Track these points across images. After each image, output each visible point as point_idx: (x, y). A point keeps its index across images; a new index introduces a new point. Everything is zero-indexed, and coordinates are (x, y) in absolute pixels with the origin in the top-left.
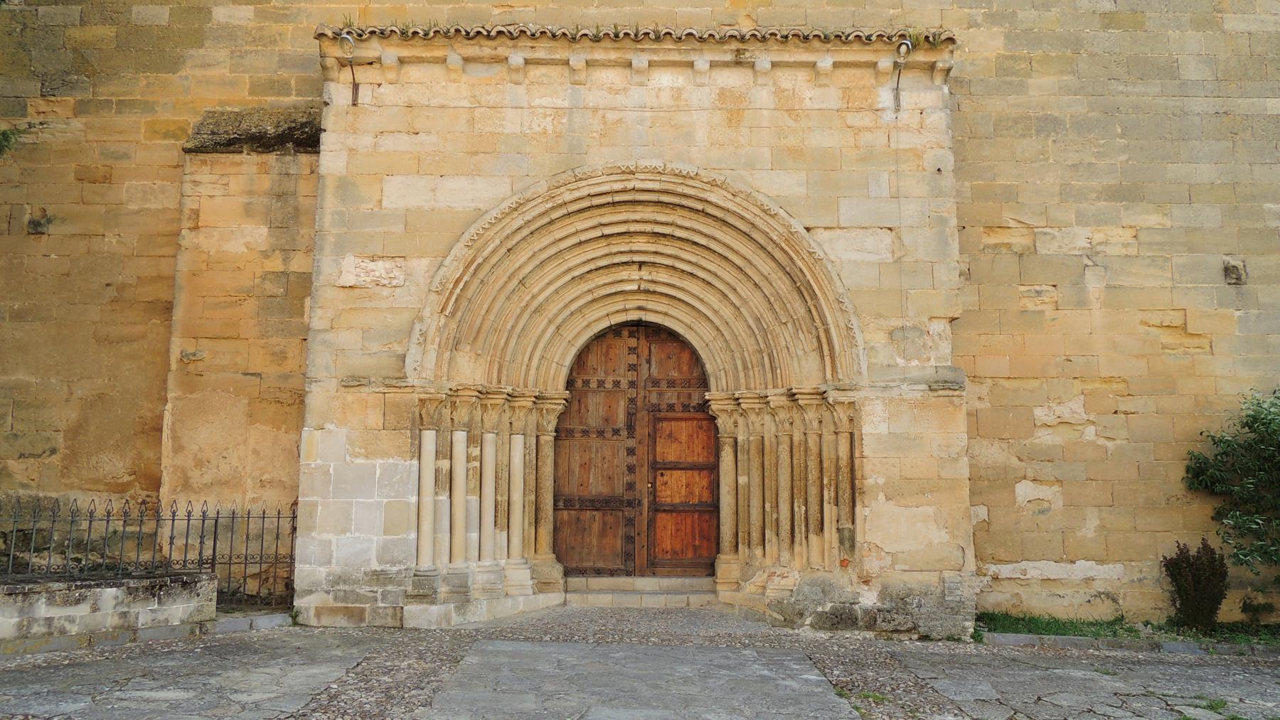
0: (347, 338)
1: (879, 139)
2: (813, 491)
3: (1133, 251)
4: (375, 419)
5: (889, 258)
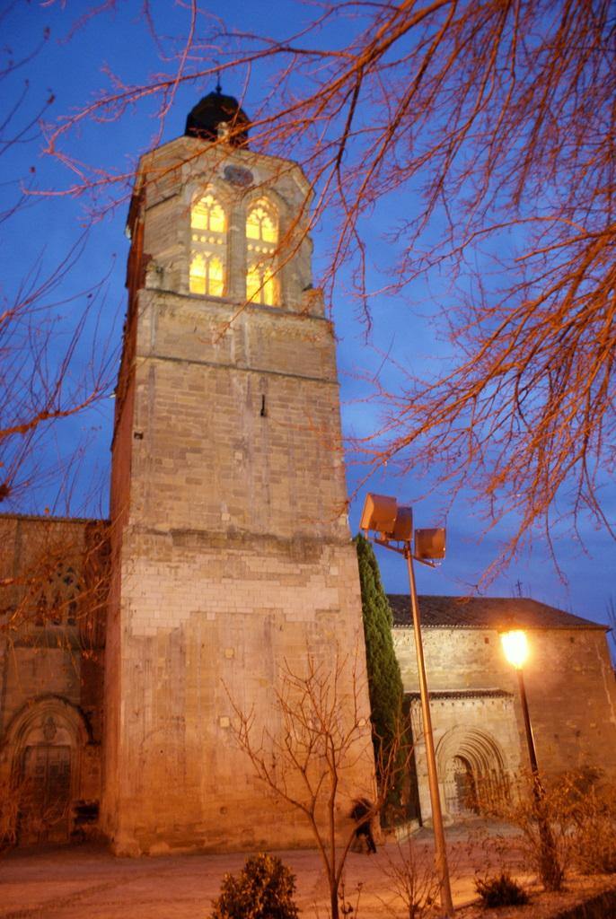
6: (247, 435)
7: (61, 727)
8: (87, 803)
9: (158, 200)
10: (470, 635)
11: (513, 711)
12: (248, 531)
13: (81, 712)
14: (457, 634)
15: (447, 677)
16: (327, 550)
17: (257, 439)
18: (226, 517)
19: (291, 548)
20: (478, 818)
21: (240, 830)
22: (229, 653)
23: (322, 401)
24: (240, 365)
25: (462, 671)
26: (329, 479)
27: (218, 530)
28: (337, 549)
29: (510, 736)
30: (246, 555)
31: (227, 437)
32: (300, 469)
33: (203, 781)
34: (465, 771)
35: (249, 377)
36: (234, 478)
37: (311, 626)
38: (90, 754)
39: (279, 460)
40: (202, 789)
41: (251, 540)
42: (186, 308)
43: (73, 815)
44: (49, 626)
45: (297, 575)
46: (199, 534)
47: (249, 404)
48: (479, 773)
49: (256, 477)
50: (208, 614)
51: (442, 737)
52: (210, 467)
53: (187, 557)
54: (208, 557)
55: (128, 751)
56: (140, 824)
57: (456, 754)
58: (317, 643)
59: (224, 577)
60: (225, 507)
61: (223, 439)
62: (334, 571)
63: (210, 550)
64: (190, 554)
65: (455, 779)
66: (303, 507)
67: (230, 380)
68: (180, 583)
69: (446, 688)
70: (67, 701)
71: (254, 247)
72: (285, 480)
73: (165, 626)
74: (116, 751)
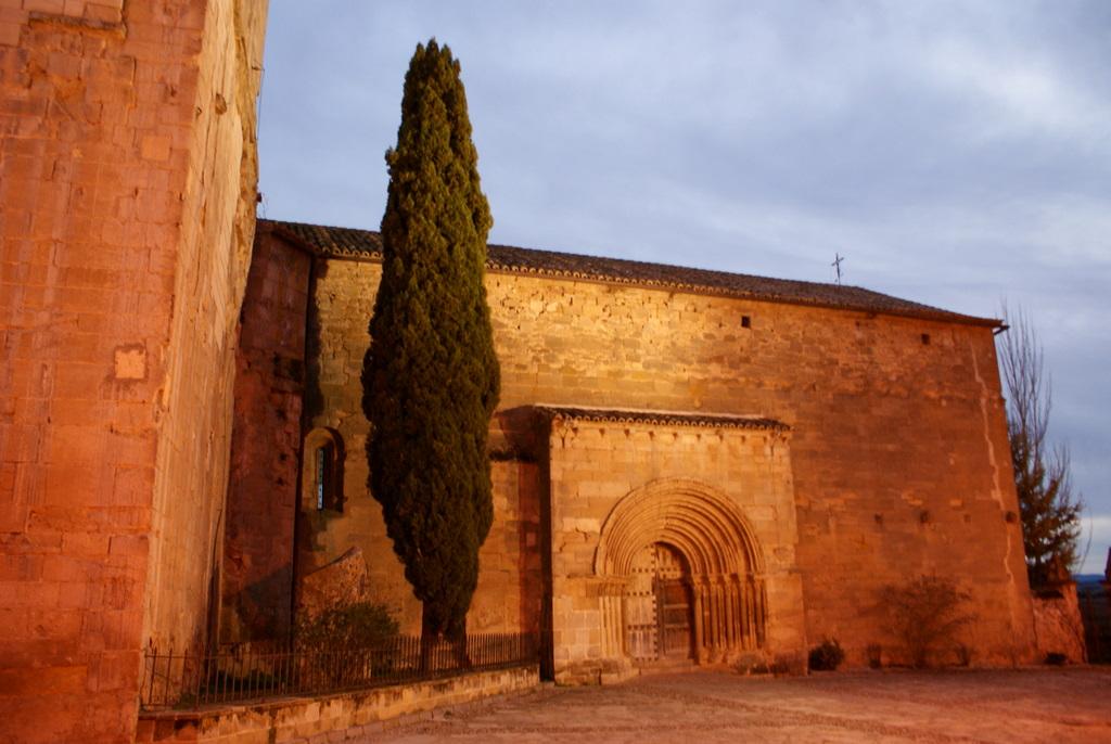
0: (568, 556)
1: (767, 469)
2: (744, 617)
3: (844, 509)
4: (582, 593)
5: (771, 518)
11: (786, 460)
25: (686, 376)
29: (774, 507)
34: (678, 574)
48: (705, 579)
51: (622, 499)
57: (659, 539)
69: (648, 406)
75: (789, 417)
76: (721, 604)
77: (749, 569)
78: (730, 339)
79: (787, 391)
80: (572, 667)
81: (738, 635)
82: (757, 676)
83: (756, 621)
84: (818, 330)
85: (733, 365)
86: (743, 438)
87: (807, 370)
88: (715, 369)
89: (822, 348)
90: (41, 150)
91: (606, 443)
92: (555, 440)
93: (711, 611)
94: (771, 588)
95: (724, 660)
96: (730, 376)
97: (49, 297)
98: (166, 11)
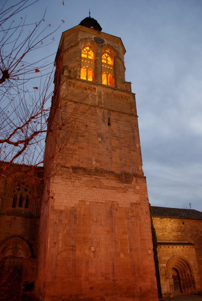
0: (162, 271)
6: (103, 132)
7: (20, 249)
8: (29, 282)
9: (69, 47)
10: (177, 221)
11: (195, 251)
12: (103, 169)
13: (28, 243)
14: (172, 220)
15: (169, 236)
16: (134, 179)
17: (106, 134)
18: (94, 163)
19: (120, 177)
20: (182, 294)
21: (99, 298)
22: (95, 219)
23: (131, 122)
24: (100, 105)
25: (175, 234)
26: (135, 151)
27: (91, 168)
28: (138, 179)
29: (194, 261)
30: (103, 179)
31: (95, 132)
32: (123, 147)
33: (83, 275)
34: (176, 274)
35: (103, 110)
36: (97, 148)
37: (128, 210)
38: (31, 261)
39: (115, 143)
40: (83, 278)
41: (105, 173)
42: (79, 83)
43: (23, 287)
44: (17, 208)
45: (123, 188)
46: (83, 169)
47: (103, 121)
48: (182, 275)
49: (106, 148)
50: (86, 202)
51: (169, 260)
52: (88, 143)
53: (78, 178)
54: (87, 178)
55: (50, 260)
56: (55, 294)
57: (173, 267)
58: (132, 217)
59: (93, 187)
60: (94, 159)
61: (94, 132)
62: (138, 188)
63: (87, 176)
64: (79, 177)
65: (173, 277)
66: (125, 161)
67: (96, 111)
68: (75, 188)
69: (169, 241)
70: (23, 239)
71: (104, 66)
72: (118, 150)
73: (68, 206)
74: (45, 258)
75: (192, 242)
76: (186, 280)
77: (190, 273)
78: (181, 227)
79: (191, 236)
80: (165, 294)
81: (190, 287)
82: (195, 296)
83: (193, 284)
84: (196, 224)
85: (182, 232)
86: (187, 247)
87: (195, 232)
88: (179, 233)
89: (197, 228)
90: (135, 222)
91: (165, 249)
92: (157, 249)
93: (184, 282)
94: (195, 277)
95: (188, 292)
96: (182, 234)
97: (139, 243)
98: (144, 201)
